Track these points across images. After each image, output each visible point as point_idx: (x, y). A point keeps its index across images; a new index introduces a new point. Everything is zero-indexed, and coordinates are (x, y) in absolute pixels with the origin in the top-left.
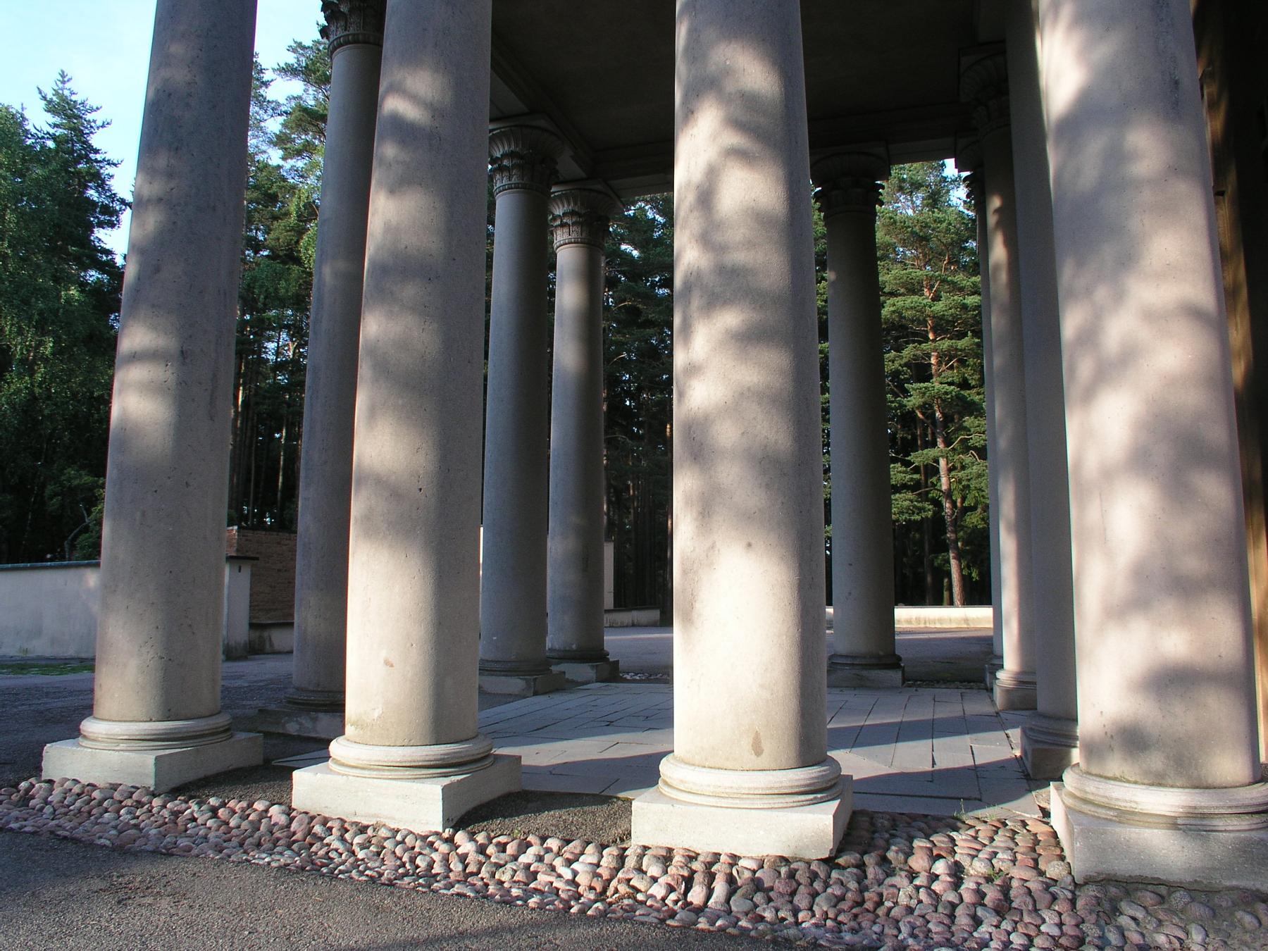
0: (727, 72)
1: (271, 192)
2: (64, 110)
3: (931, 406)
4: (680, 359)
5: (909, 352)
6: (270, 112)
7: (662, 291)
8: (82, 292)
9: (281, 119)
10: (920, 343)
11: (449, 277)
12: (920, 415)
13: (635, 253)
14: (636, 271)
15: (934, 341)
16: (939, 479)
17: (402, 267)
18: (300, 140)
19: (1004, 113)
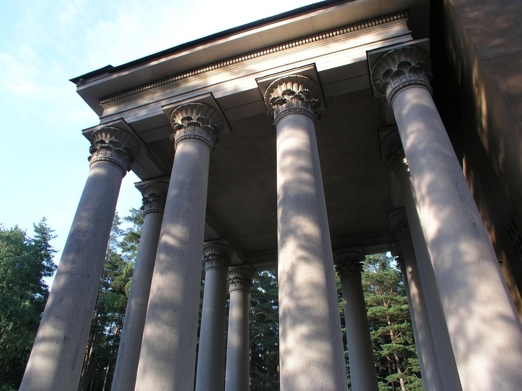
0: (298, 227)
1: (116, 264)
2: (41, 231)
3: (393, 354)
4: (282, 347)
5: (380, 330)
6: (120, 234)
7: (274, 307)
8: (31, 303)
9: (124, 237)
10: (385, 326)
11: (183, 312)
12: (389, 359)
13: (263, 291)
14: (264, 299)
15: (391, 325)
16: (401, 388)
17: (164, 305)
18: (130, 245)
19: (408, 234)
